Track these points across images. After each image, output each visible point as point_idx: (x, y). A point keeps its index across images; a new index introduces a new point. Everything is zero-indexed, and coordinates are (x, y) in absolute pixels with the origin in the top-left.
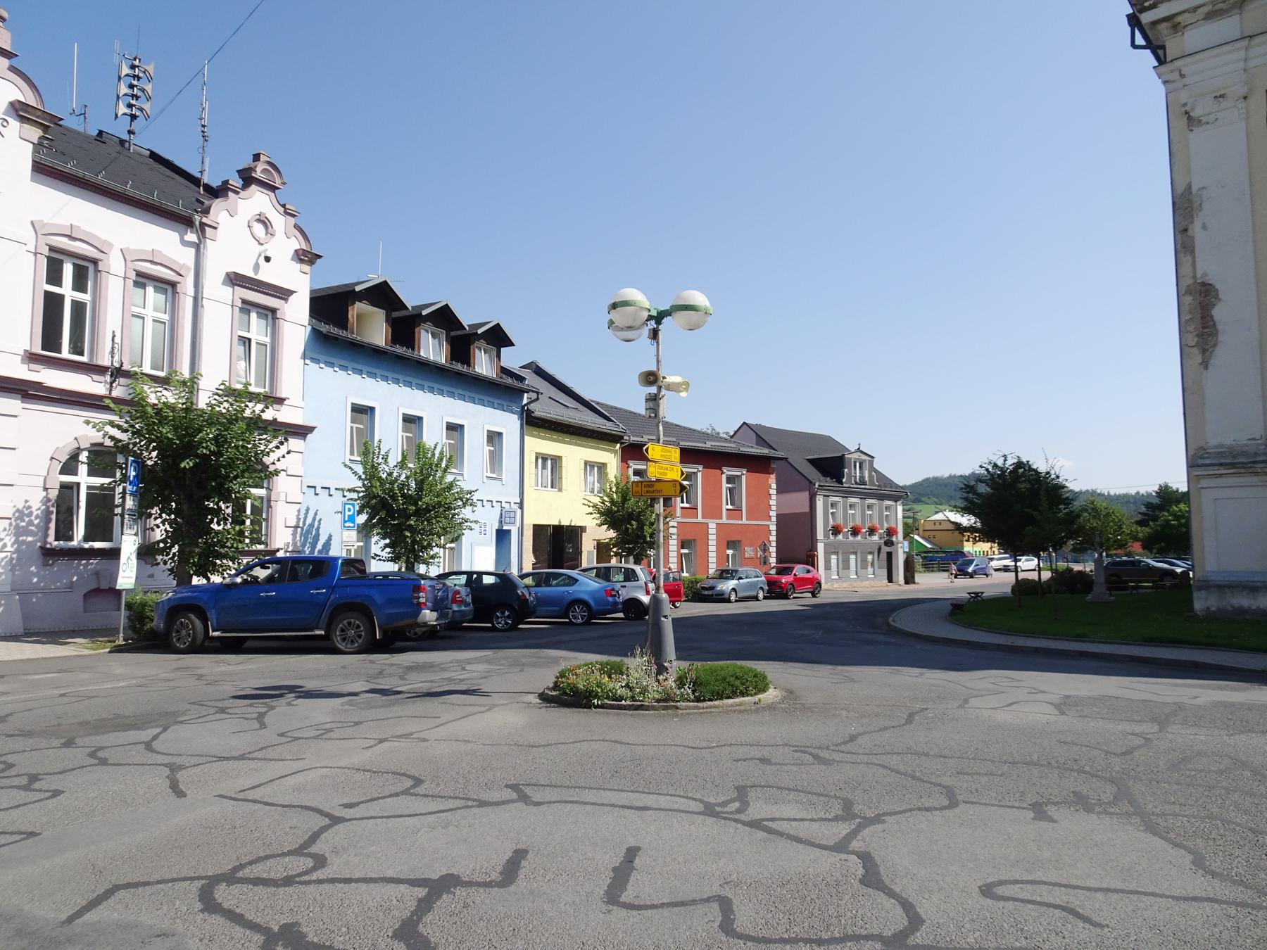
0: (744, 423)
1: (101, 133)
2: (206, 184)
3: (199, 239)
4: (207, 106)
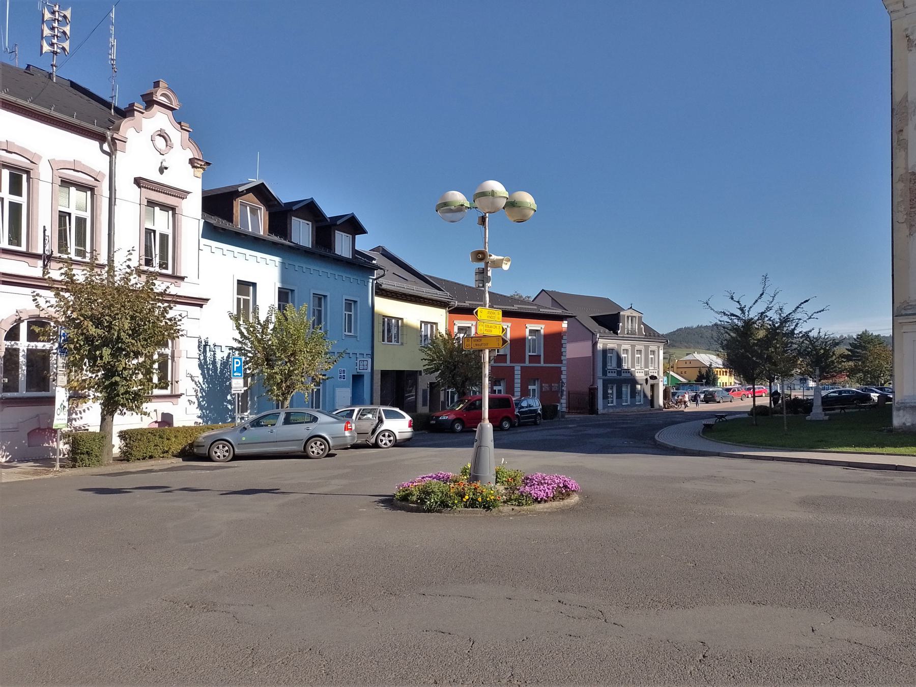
0: (543, 290)
1: (29, 66)
2: (116, 107)
3: (111, 149)
4: (115, 44)
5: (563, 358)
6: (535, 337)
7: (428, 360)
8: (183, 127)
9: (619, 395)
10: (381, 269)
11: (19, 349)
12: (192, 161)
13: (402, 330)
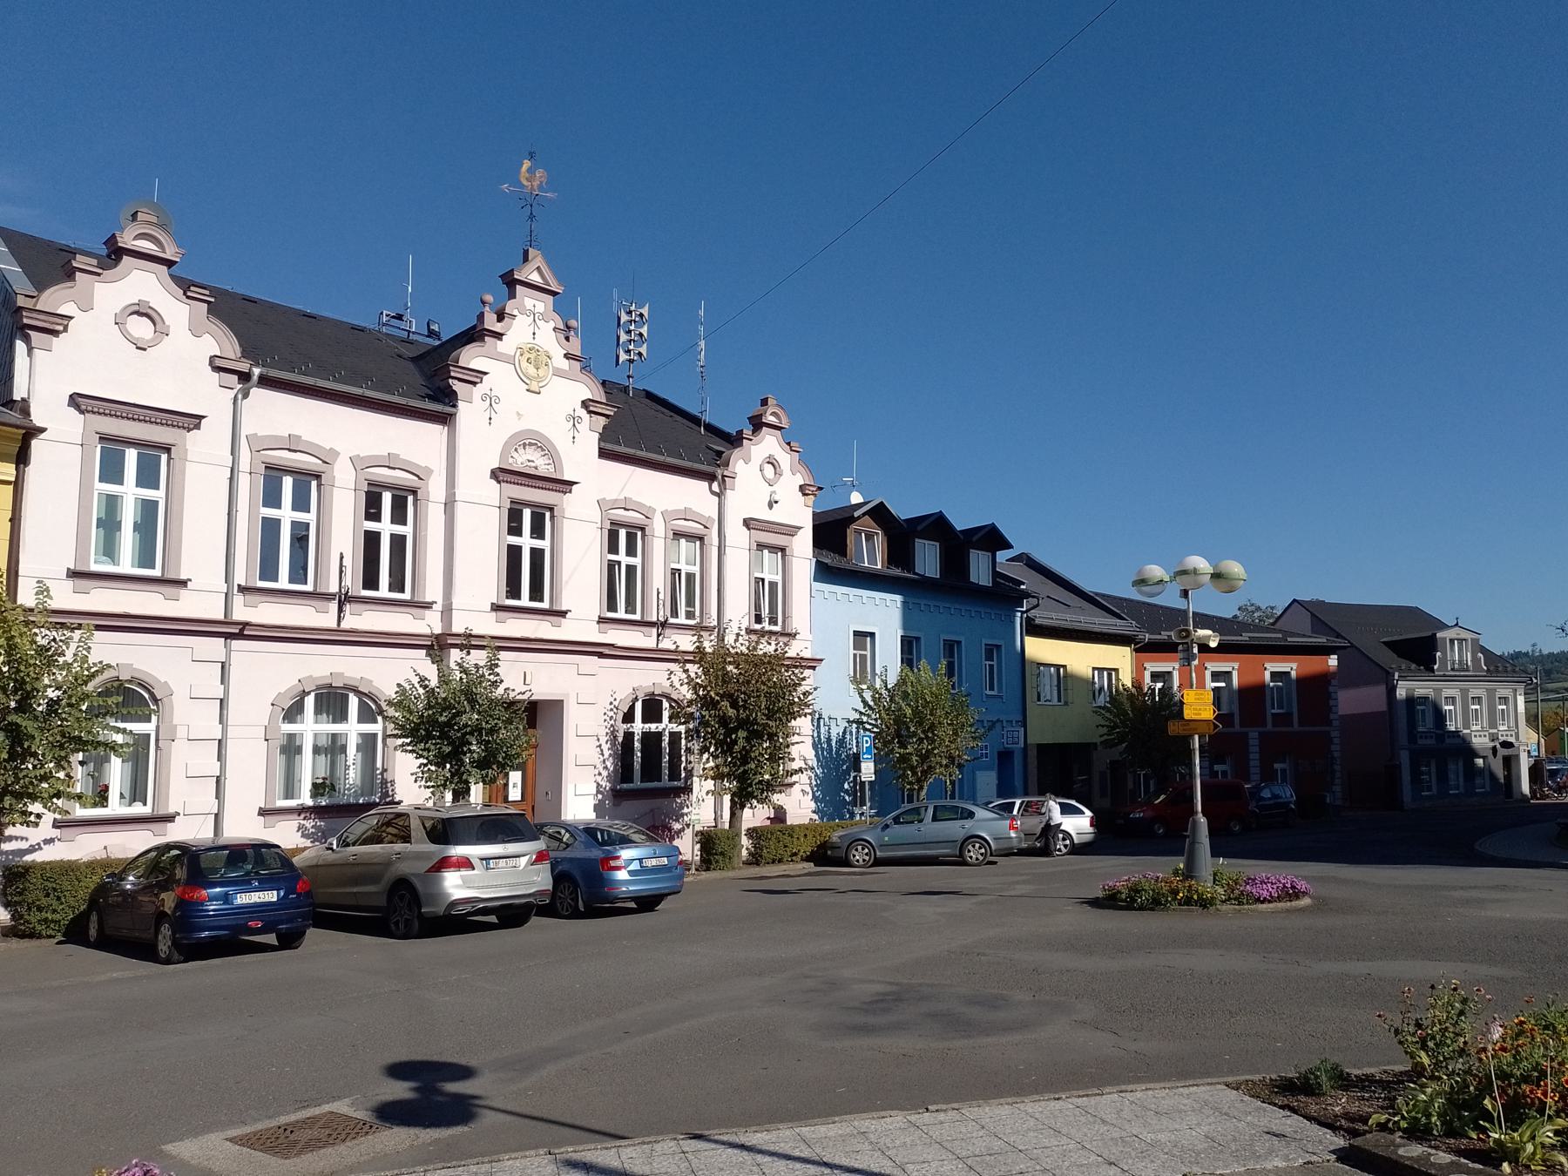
0: (1295, 600)
3: (720, 489)
5: (1332, 716)
6: (1280, 684)
7: (1107, 726)
8: (793, 448)
9: (1443, 777)
10: (1034, 597)
11: (634, 733)
12: (802, 488)
13: (1066, 683)
